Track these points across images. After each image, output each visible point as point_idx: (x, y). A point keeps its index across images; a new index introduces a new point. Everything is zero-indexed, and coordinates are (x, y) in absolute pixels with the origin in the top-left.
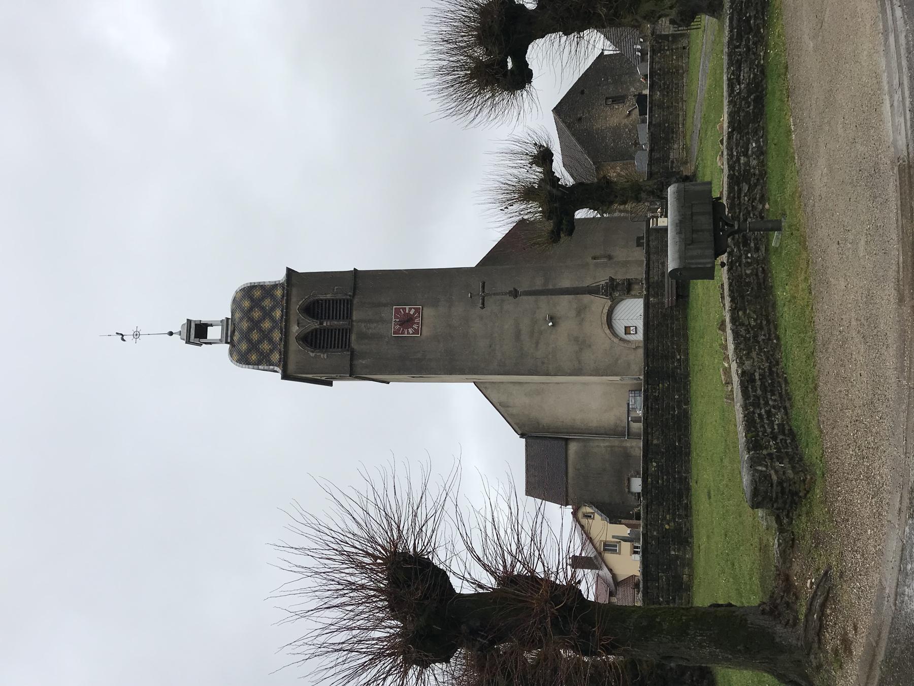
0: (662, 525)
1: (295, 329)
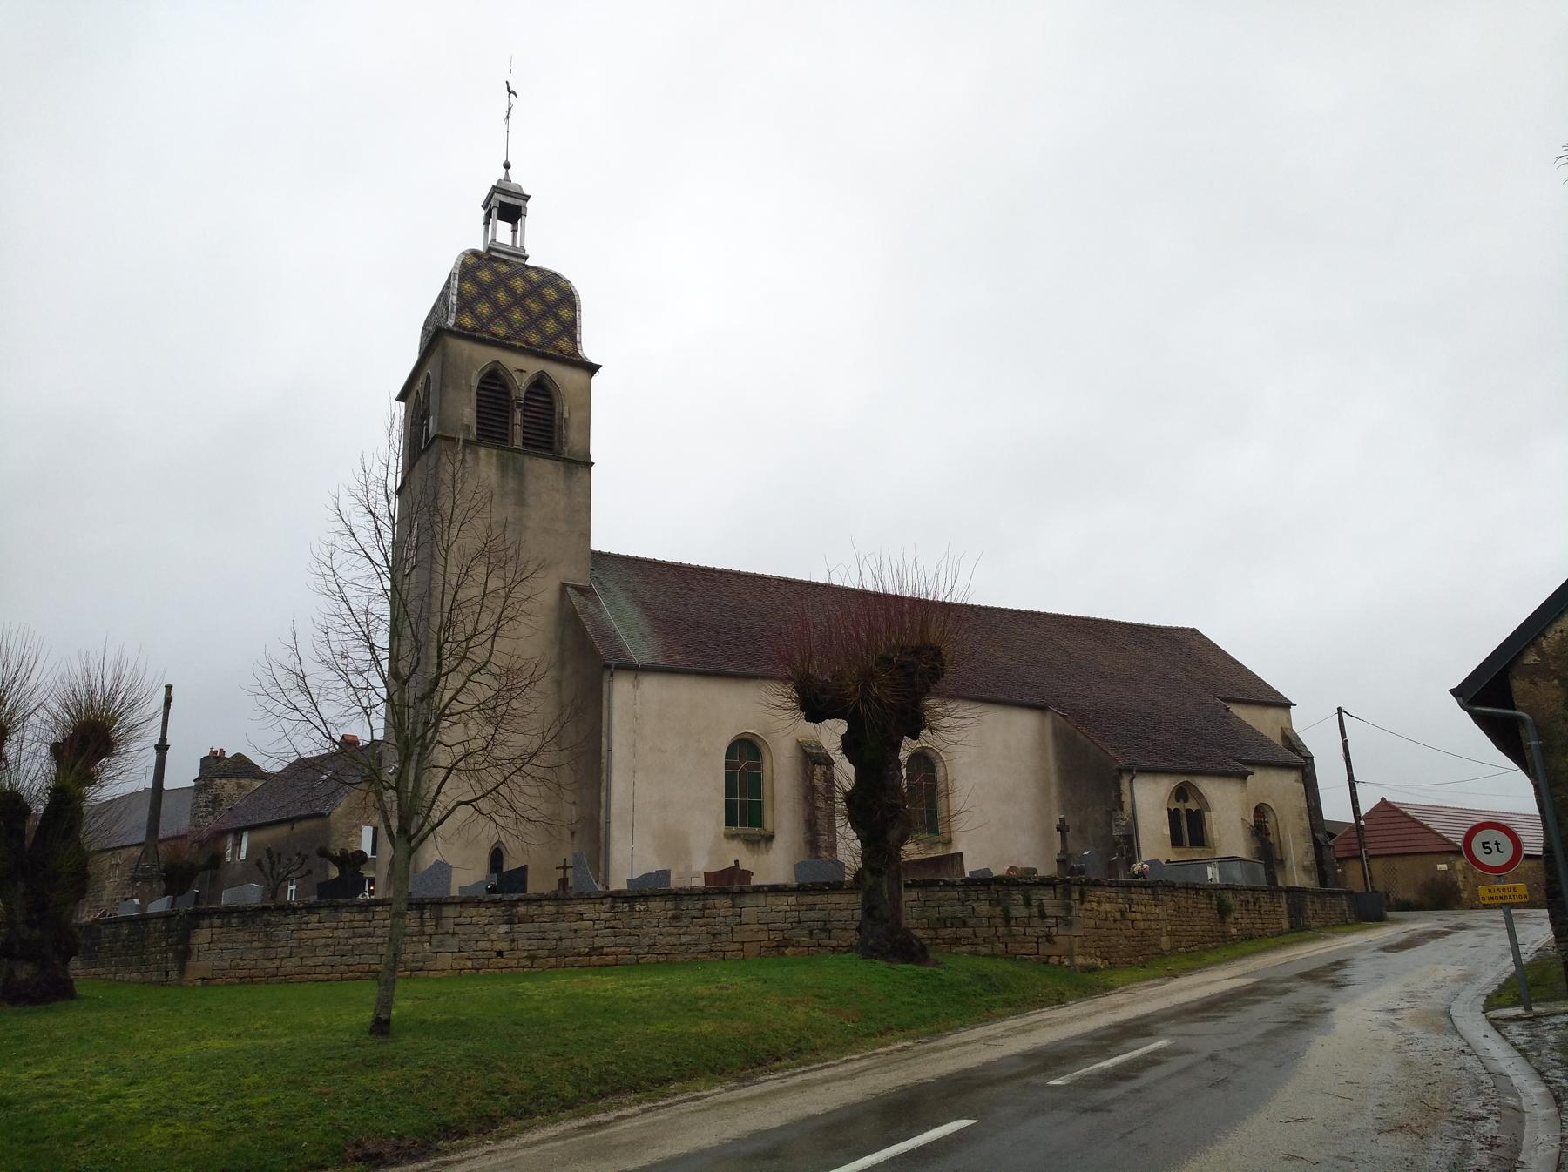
1: (512, 361)
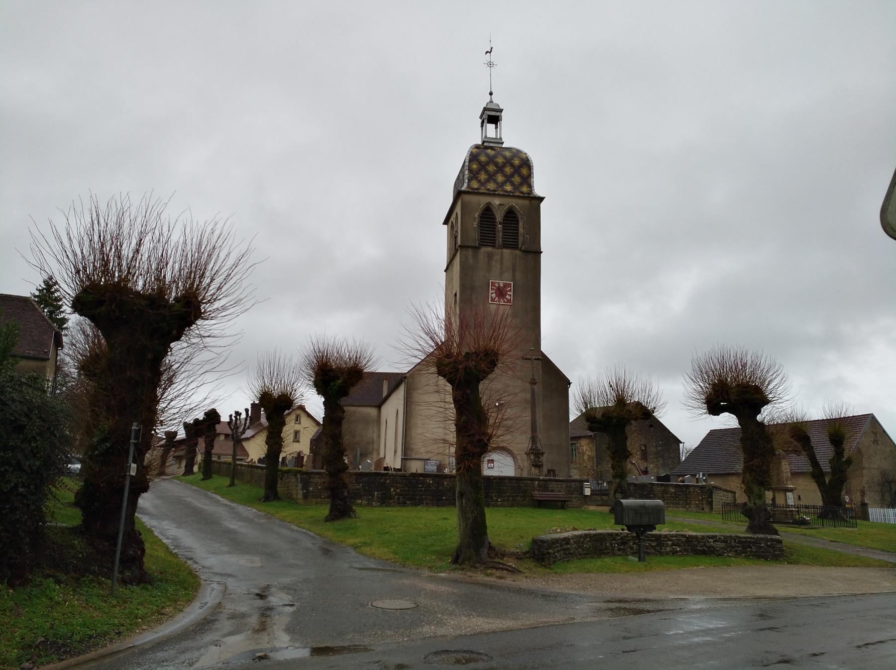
0: (393, 486)
1: (496, 201)
